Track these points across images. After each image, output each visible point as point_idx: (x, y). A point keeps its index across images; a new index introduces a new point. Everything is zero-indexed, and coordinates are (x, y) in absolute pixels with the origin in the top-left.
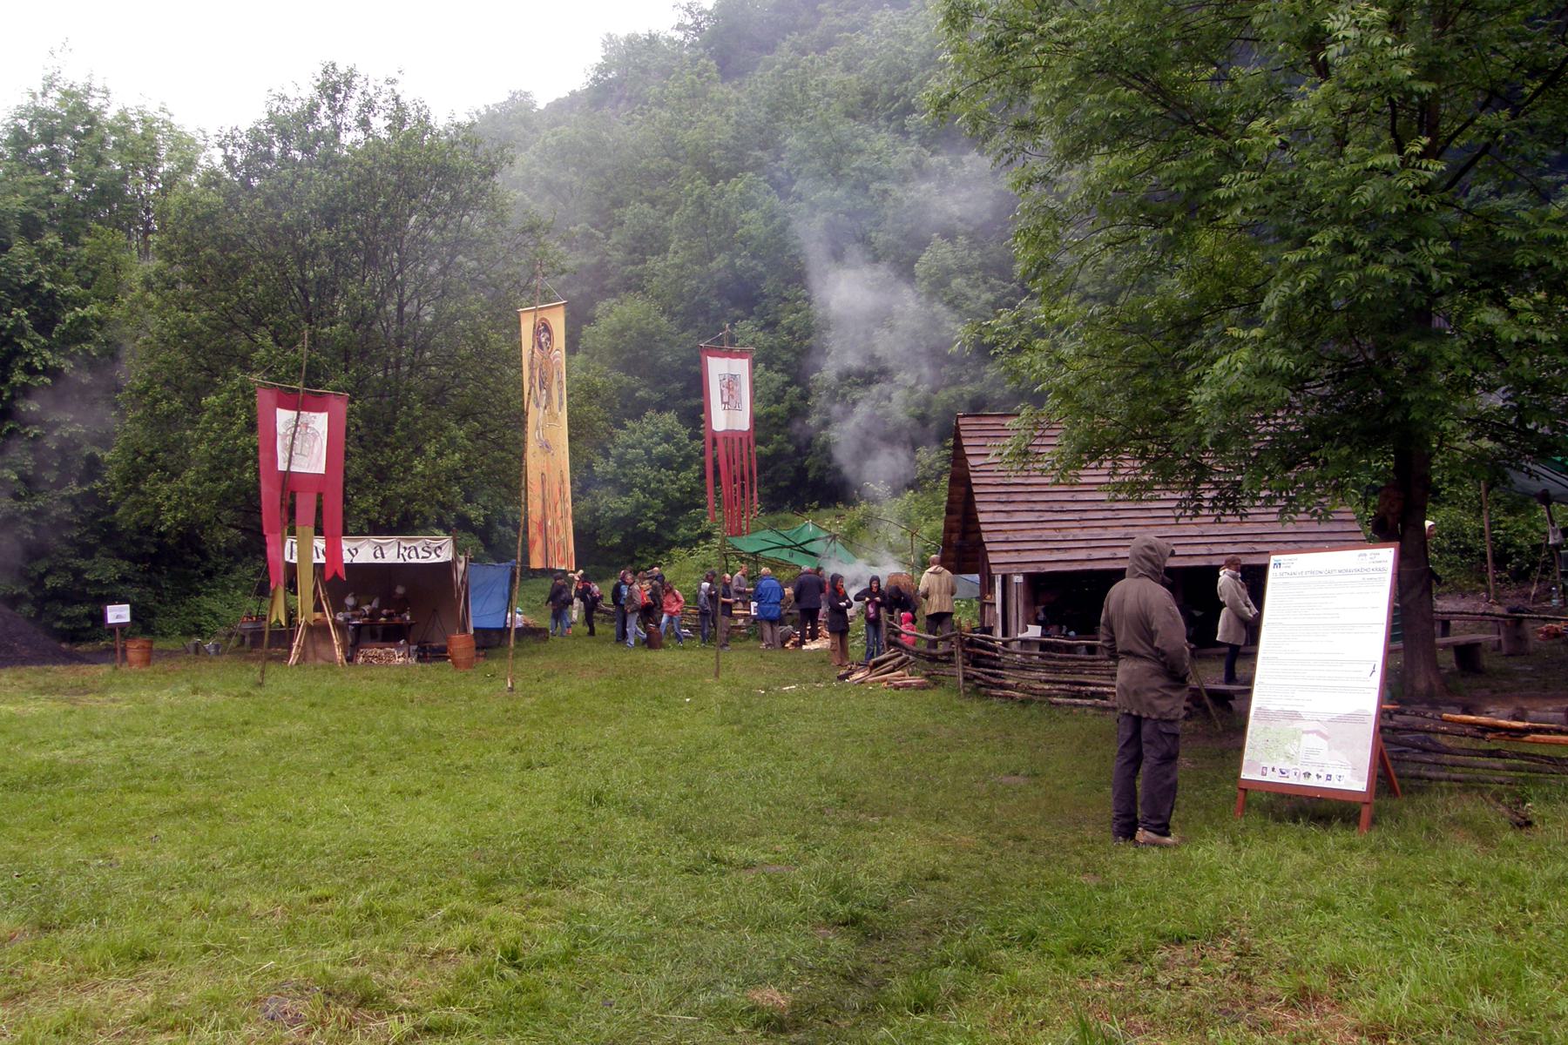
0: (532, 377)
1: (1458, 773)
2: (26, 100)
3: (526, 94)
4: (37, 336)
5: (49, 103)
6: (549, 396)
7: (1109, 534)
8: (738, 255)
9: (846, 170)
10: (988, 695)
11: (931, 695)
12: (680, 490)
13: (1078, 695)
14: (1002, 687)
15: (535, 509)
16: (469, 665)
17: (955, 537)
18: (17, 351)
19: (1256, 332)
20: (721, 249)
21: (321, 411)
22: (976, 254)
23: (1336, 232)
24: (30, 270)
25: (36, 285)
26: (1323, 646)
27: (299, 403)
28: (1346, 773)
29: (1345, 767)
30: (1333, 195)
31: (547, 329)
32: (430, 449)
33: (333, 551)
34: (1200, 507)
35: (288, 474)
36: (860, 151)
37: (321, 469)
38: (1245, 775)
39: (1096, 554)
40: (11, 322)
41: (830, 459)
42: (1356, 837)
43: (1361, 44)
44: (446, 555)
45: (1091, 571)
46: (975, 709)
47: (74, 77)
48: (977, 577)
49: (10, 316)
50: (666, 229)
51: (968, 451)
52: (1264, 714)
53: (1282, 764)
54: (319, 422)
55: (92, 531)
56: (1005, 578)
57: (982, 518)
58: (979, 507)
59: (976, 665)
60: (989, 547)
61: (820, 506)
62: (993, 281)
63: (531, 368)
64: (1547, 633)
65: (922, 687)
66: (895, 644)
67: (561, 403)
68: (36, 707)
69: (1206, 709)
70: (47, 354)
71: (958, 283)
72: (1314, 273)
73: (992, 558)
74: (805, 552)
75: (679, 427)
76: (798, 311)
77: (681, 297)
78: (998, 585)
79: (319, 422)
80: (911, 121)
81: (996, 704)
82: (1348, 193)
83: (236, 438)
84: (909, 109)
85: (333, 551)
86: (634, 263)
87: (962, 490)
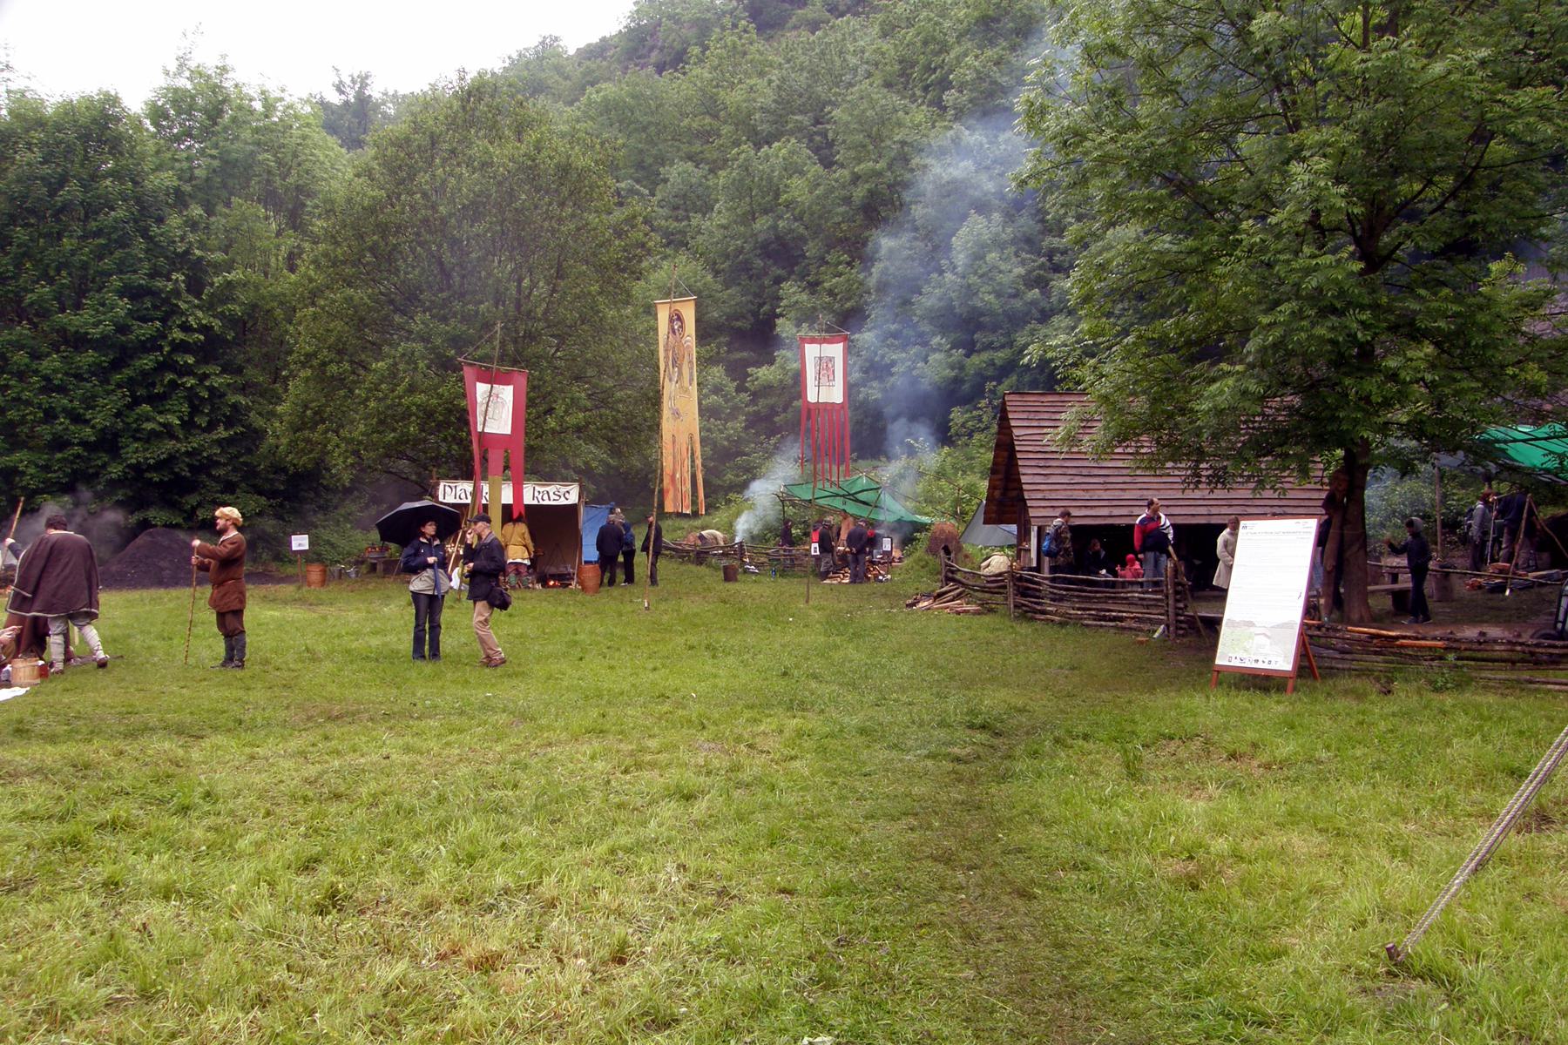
0: (666, 357)
1: (1355, 665)
2: (162, 82)
3: (556, 39)
4: (191, 298)
5: (183, 83)
6: (680, 373)
7: (1127, 495)
8: (781, 217)
9: (888, 143)
10: (1033, 619)
11: (987, 619)
12: (727, 439)
13: (1104, 618)
14: (1044, 612)
15: (668, 464)
16: (597, 592)
17: (997, 493)
18: (175, 310)
19: (1239, 368)
20: (766, 212)
21: (508, 384)
22: (1009, 230)
23: (1293, 305)
24: (182, 239)
25: (187, 252)
26: (1270, 576)
27: (492, 379)
28: (1280, 659)
29: (1280, 656)
30: (1294, 277)
31: (679, 318)
32: (560, 408)
33: (518, 494)
34: (1199, 482)
35: (482, 435)
36: (900, 124)
37: (508, 431)
38: (1218, 661)
39: (1116, 512)
40: (170, 286)
41: (41, 123)
42: (1284, 697)
43: (1311, 184)
44: (573, 498)
45: (1112, 526)
46: (1024, 629)
47: (206, 59)
48: (1014, 528)
49: (169, 280)
50: (708, 187)
51: (1013, 423)
52: (1232, 623)
53: (1244, 655)
54: (506, 393)
55: (235, 470)
56: (1040, 529)
57: (1024, 479)
58: (1022, 470)
59: (1024, 595)
60: (1029, 503)
61: (859, 457)
62: (1024, 255)
63: (666, 350)
64: (1472, 586)
65: (977, 613)
66: (953, 580)
67: (691, 380)
68: (294, 613)
69: (1198, 631)
70: (200, 314)
71: (992, 256)
72: (1278, 332)
73: (1032, 513)
74: (857, 500)
75: (726, 380)
76: (840, 275)
77: (727, 257)
78: (1034, 535)
79: (506, 393)
80: (949, 97)
81: (1038, 625)
82: (1302, 278)
83: (400, 397)
84: (945, 84)
85: (518, 494)
86: (677, 219)
87: (1006, 454)
